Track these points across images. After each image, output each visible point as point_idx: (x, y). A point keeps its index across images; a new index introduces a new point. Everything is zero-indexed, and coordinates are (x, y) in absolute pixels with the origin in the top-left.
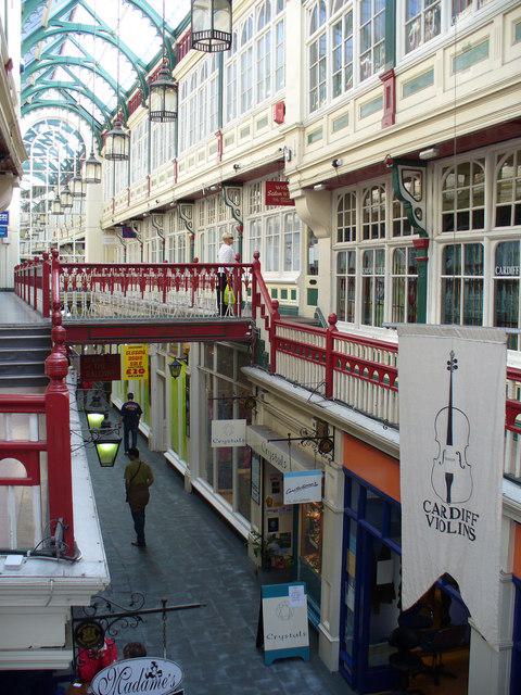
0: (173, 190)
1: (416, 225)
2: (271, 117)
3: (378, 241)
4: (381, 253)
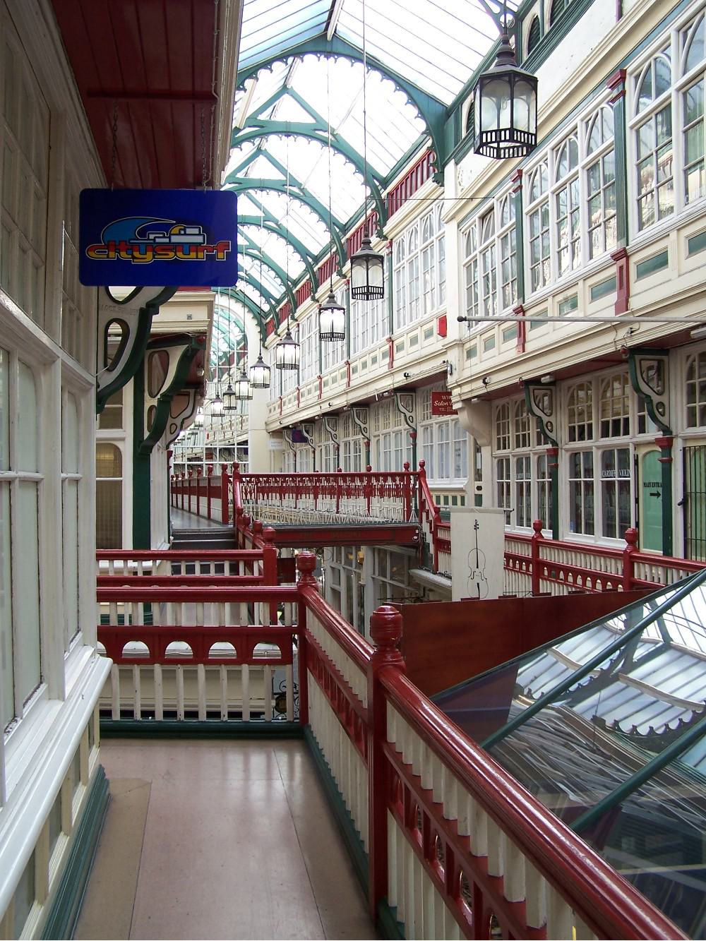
0: (347, 393)
1: (546, 437)
2: (436, 331)
3: (586, 443)
4: (588, 455)
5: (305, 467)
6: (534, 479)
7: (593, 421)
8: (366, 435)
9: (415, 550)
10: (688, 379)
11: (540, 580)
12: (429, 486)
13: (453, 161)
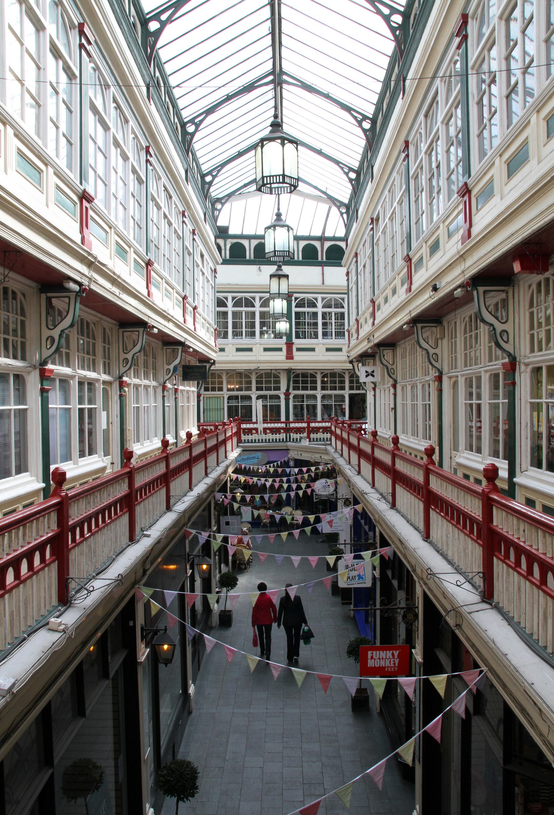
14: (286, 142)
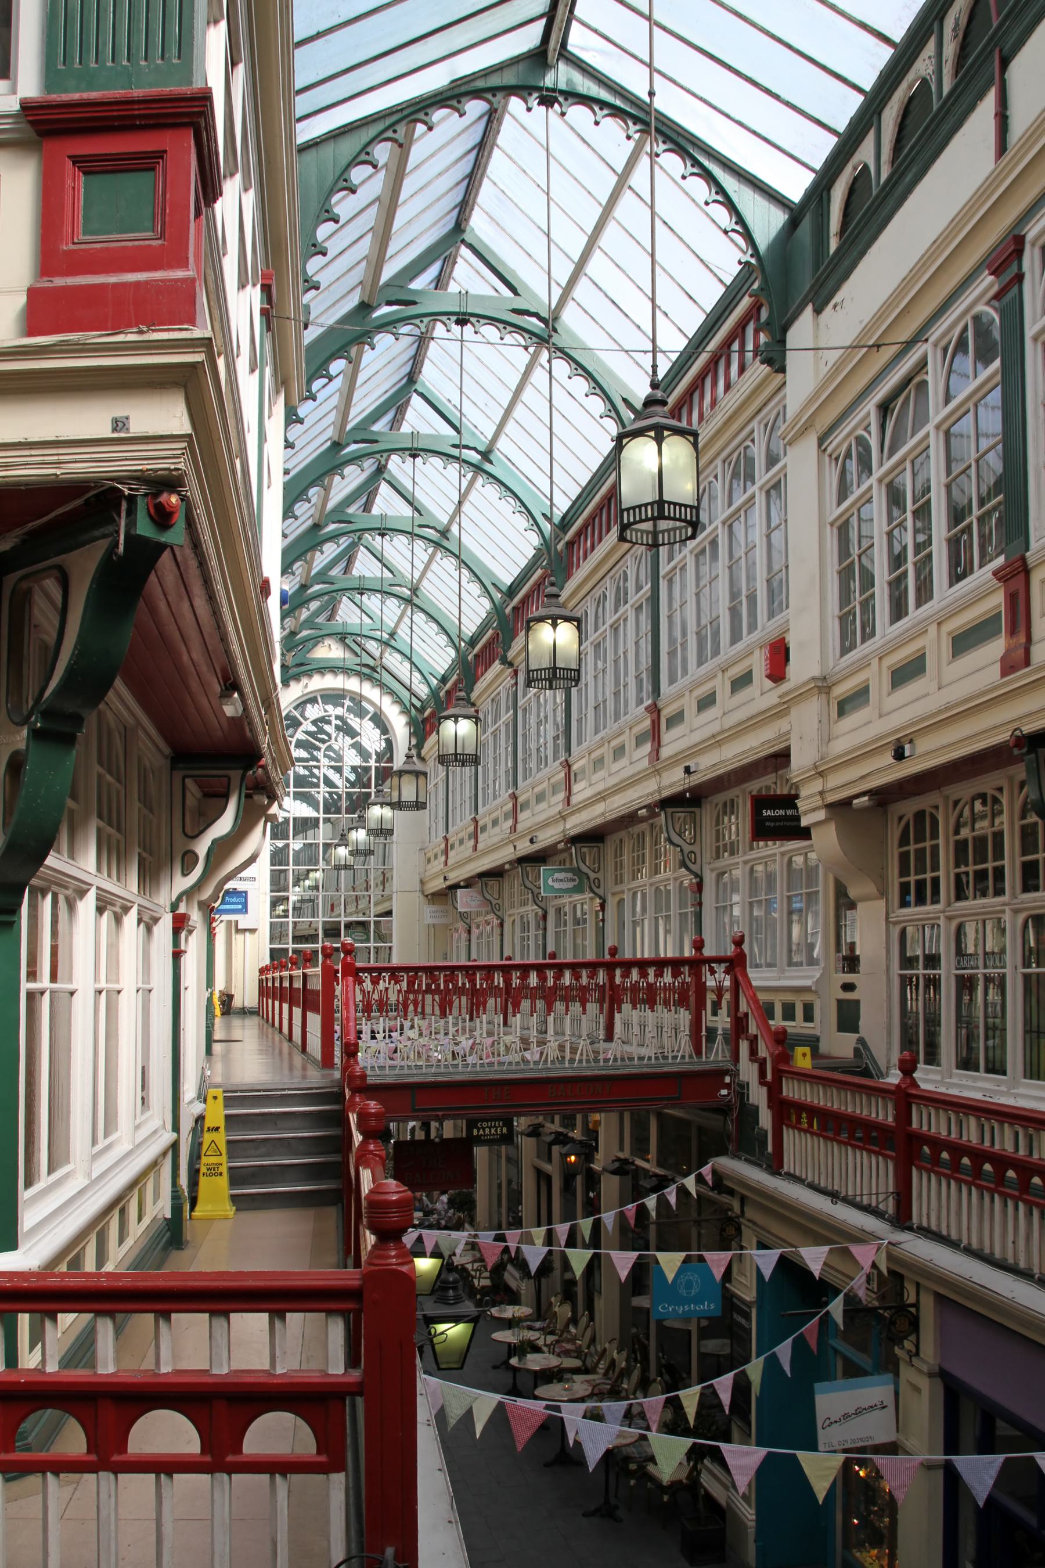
5: (485, 951)
6: (949, 971)
7: (941, 873)
8: (600, 891)
9: (721, 1118)
10: (901, 845)
11: (784, 1128)
12: (754, 983)
13: (809, 309)
14: (666, 433)
